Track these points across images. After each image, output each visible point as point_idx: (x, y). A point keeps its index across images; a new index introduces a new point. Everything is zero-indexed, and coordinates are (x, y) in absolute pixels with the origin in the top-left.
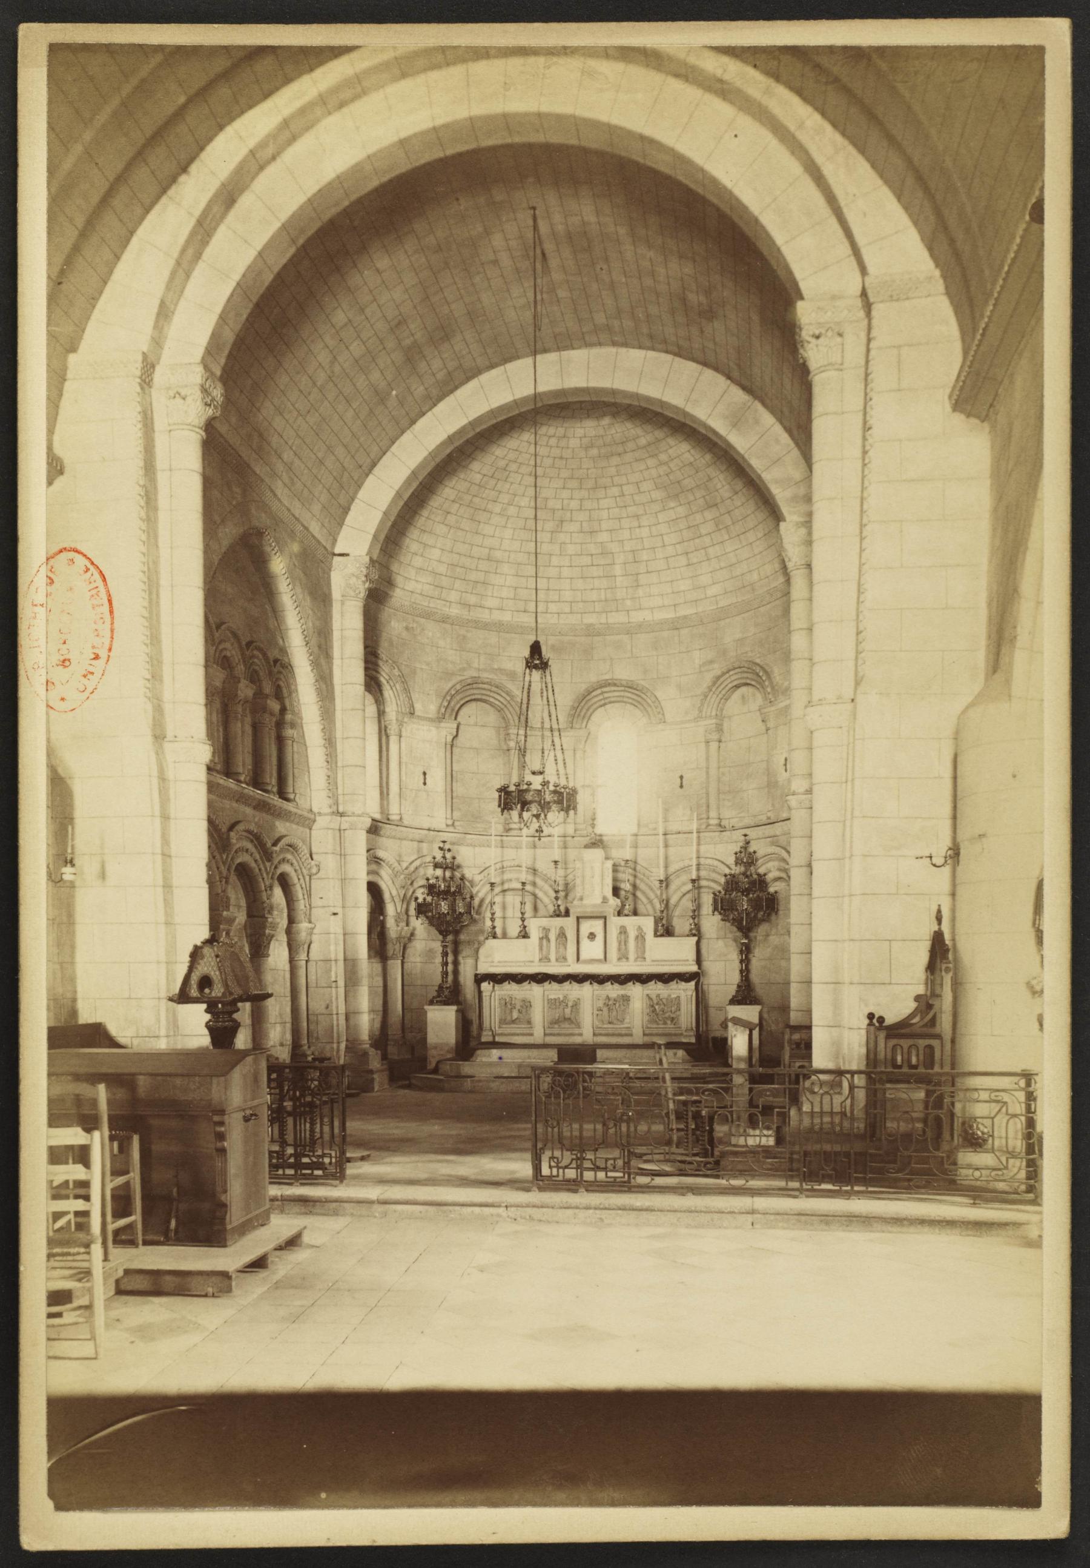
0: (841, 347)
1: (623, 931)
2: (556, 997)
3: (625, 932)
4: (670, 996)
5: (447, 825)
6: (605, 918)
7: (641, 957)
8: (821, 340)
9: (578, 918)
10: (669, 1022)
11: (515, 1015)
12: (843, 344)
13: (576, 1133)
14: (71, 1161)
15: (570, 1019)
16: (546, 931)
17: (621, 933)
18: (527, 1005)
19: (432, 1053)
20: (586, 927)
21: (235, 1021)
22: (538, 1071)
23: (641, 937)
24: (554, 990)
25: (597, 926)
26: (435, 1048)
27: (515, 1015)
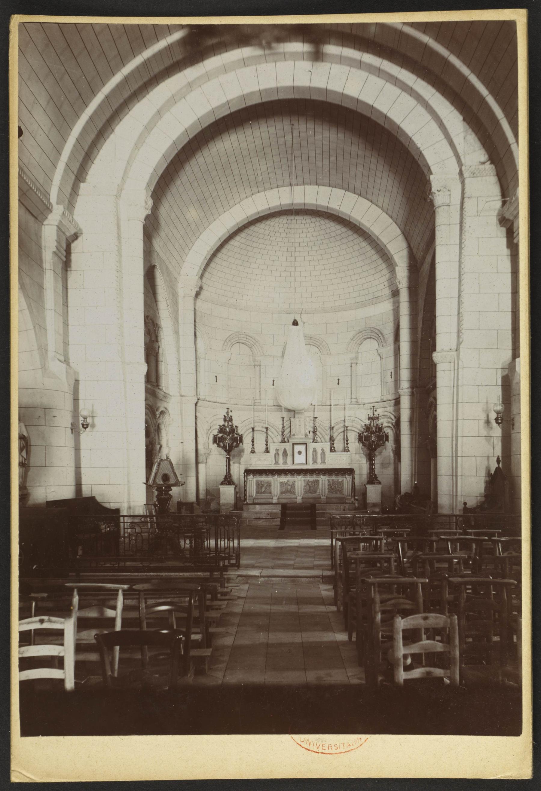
0: (449, 196)
1: (315, 450)
2: (284, 481)
3: (316, 451)
4: (338, 480)
5: (227, 401)
6: (306, 444)
7: (323, 462)
8: (440, 193)
9: (293, 444)
10: (338, 492)
11: (263, 490)
12: (450, 195)
13: (236, 545)
14: (520, 538)
15: (290, 491)
16: (277, 450)
17: (313, 451)
18: (269, 485)
19: (223, 507)
20: (297, 448)
21: (170, 495)
22: (272, 516)
23: (323, 453)
24: (284, 479)
25: (302, 448)
26: (224, 505)
27: (263, 490)
